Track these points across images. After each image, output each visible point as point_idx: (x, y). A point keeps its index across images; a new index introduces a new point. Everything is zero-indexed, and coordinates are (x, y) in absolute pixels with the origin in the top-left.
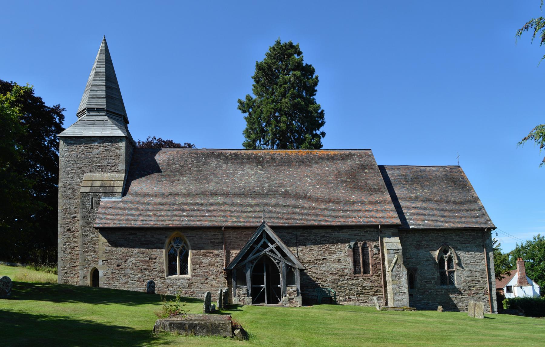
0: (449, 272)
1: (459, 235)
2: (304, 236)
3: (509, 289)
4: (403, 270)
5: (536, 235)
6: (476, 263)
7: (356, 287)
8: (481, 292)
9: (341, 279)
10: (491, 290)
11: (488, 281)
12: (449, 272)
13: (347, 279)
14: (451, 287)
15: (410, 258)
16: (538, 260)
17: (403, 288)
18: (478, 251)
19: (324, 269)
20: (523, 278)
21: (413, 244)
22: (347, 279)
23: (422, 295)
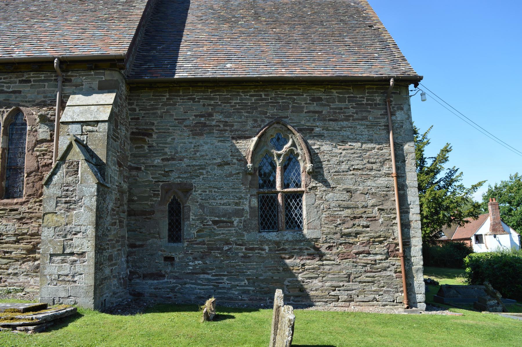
0: (287, 196)
3: (479, 239)
4: (83, 181)
5: (513, 174)
6: (366, 172)
8: (378, 248)
10: (407, 244)
11: (398, 220)
12: (287, 196)
14: (289, 235)
15: (173, 159)
16: (515, 204)
17: (77, 240)
18: (371, 141)
20: (497, 224)
21: (187, 123)
23: (202, 258)
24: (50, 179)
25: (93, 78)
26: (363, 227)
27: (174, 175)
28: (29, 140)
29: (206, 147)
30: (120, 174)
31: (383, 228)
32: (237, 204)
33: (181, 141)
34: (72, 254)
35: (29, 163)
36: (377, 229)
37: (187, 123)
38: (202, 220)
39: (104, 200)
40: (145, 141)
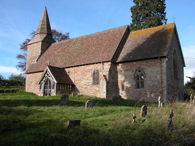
30: (113, 79)
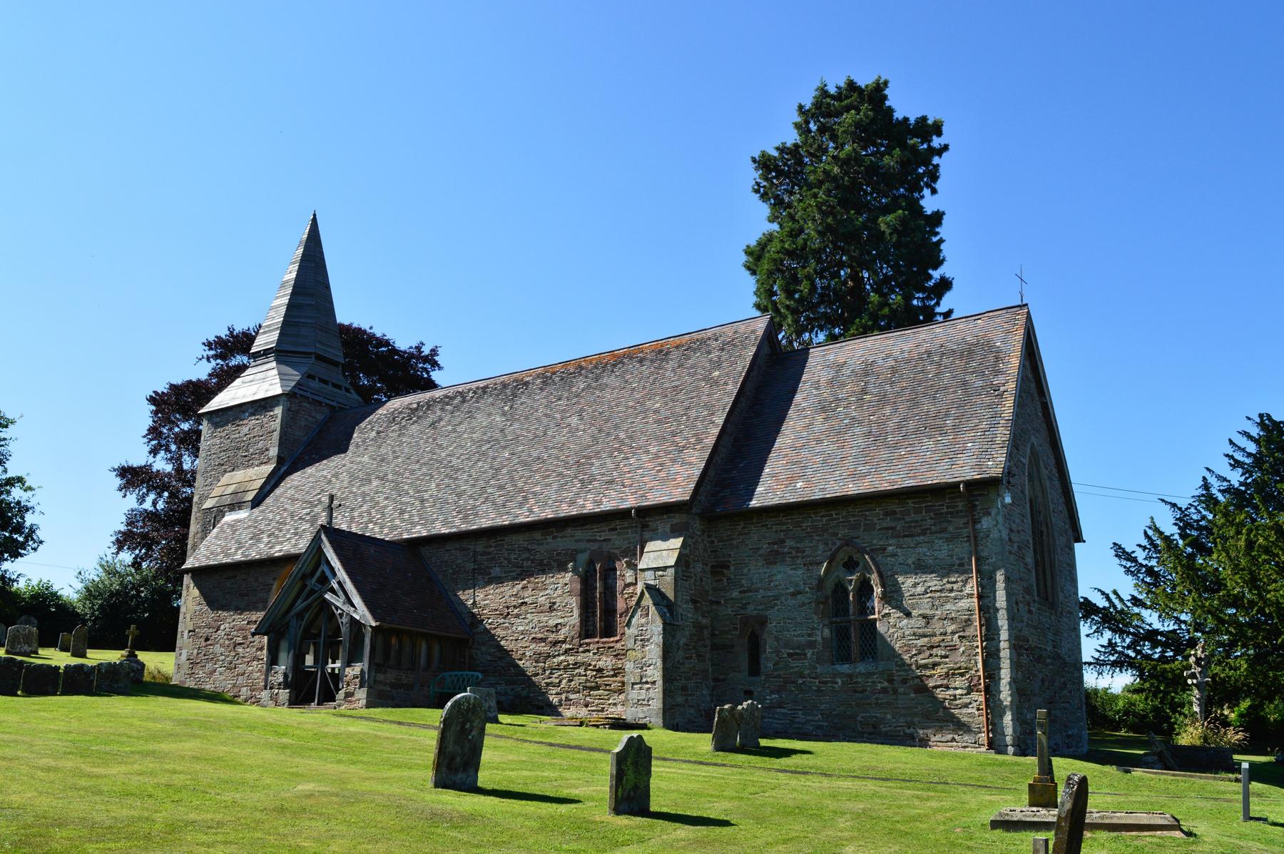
1: (894, 513)
2: (489, 553)
7: (581, 671)
8: (958, 682)
9: (552, 651)
13: (566, 652)
15: (749, 590)
17: (650, 671)
19: (521, 628)
21: (761, 552)
22: (566, 652)
23: (778, 692)
24: (630, 621)
25: (663, 525)
26: (942, 657)
27: (751, 607)
28: (620, 584)
29: (779, 577)
30: (696, 609)
31: (964, 659)
32: (810, 635)
33: (756, 571)
34: (647, 683)
35: (621, 605)
36: (959, 659)
37: (761, 552)
38: (778, 653)
39: (674, 637)
40: (723, 574)
